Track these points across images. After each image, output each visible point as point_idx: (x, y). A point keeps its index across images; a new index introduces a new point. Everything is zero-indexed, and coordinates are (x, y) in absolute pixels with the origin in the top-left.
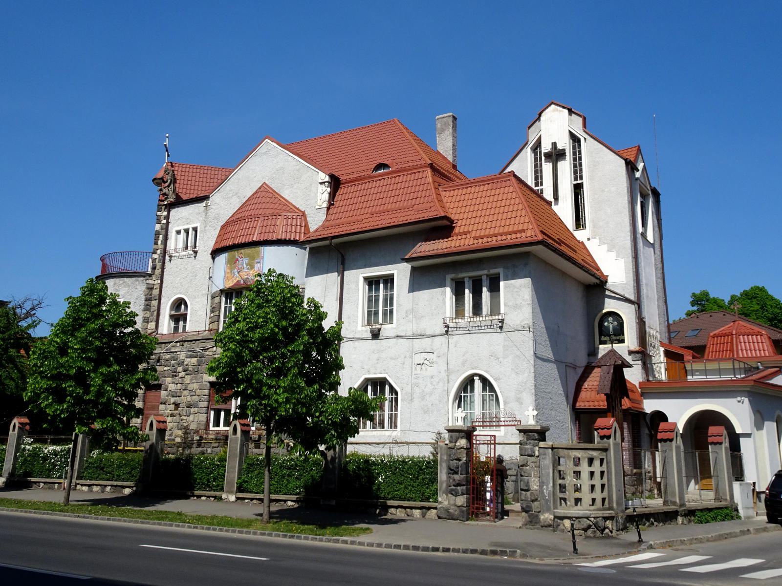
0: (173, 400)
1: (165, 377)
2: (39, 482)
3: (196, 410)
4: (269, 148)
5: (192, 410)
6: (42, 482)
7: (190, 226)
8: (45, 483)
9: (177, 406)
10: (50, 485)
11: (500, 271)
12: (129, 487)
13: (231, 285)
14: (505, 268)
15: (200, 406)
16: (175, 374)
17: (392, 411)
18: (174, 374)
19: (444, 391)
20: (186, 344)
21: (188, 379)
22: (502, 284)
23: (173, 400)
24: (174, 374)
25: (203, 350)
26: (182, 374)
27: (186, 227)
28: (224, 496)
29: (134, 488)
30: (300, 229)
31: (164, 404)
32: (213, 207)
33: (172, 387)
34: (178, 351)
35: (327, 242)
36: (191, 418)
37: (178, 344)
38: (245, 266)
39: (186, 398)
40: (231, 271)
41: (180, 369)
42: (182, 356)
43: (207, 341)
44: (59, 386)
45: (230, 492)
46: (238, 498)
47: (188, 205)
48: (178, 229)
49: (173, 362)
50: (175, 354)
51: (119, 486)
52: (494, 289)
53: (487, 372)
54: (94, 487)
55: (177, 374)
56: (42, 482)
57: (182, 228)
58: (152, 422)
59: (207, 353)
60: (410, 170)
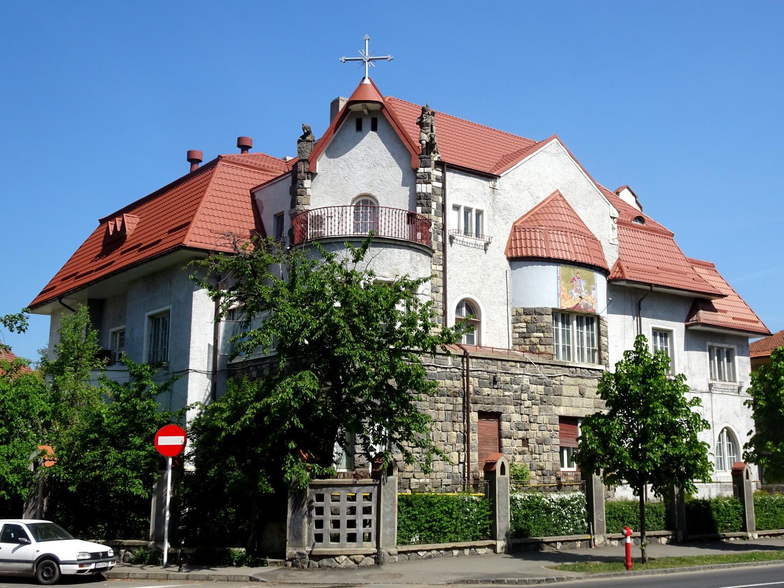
0: (521, 434)
1: (506, 404)
2: (555, 542)
3: (548, 447)
4: (559, 151)
5: (546, 447)
6: (559, 541)
7: (475, 207)
8: (562, 542)
9: (525, 441)
10: (569, 544)
11: (734, 347)
12: (664, 536)
13: (569, 306)
14: (738, 345)
15: (553, 443)
16: (519, 401)
17: (730, 455)
18: (518, 402)
19: (711, 439)
20: (528, 366)
21: (535, 410)
22: (737, 358)
23: (521, 434)
24: (518, 402)
25: (549, 377)
26: (528, 403)
27: (469, 205)
28: (750, 535)
29: (670, 537)
30: (521, 243)
31: (510, 438)
32: (502, 193)
33: (516, 418)
34: (521, 374)
35: (648, 288)
36: (545, 456)
37: (518, 364)
38: (583, 290)
39: (534, 433)
40: (568, 290)
41: (524, 396)
42: (526, 381)
43: (553, 367)
44: (317, 403)
45: (752, 531)
46: (759, 536)
47: (469, 176)
48: (458, 203)
49: (515, 387)
50: (516, 376)
51: (655, 536)
52: (730, 359)
53: (733, 426)
54: (343, 556)
55: (522, 402)
56: (559, 541)
57: (464, 204)
58: (503, 463)
59: (554, 381)
60: (660, 233)
